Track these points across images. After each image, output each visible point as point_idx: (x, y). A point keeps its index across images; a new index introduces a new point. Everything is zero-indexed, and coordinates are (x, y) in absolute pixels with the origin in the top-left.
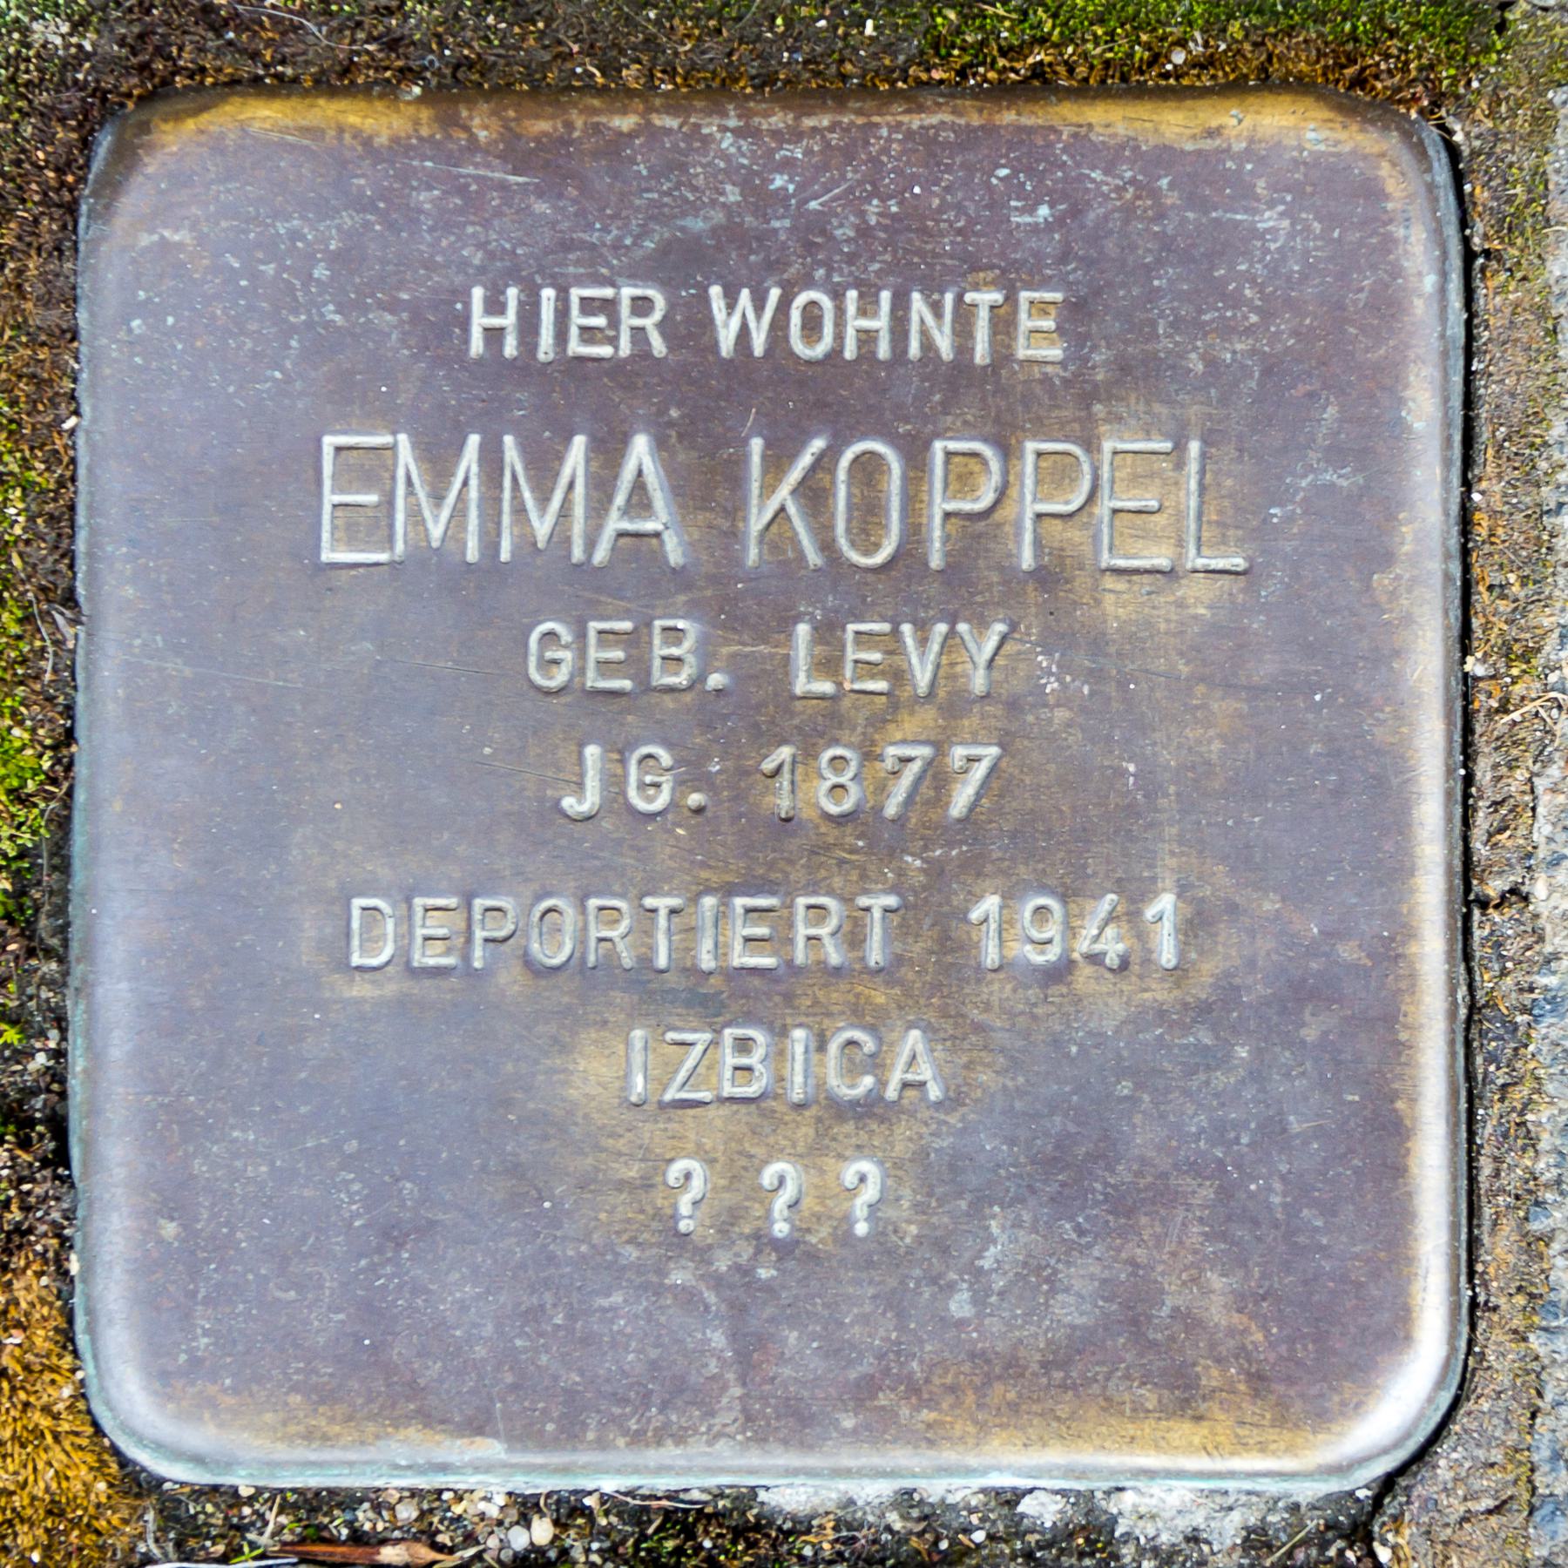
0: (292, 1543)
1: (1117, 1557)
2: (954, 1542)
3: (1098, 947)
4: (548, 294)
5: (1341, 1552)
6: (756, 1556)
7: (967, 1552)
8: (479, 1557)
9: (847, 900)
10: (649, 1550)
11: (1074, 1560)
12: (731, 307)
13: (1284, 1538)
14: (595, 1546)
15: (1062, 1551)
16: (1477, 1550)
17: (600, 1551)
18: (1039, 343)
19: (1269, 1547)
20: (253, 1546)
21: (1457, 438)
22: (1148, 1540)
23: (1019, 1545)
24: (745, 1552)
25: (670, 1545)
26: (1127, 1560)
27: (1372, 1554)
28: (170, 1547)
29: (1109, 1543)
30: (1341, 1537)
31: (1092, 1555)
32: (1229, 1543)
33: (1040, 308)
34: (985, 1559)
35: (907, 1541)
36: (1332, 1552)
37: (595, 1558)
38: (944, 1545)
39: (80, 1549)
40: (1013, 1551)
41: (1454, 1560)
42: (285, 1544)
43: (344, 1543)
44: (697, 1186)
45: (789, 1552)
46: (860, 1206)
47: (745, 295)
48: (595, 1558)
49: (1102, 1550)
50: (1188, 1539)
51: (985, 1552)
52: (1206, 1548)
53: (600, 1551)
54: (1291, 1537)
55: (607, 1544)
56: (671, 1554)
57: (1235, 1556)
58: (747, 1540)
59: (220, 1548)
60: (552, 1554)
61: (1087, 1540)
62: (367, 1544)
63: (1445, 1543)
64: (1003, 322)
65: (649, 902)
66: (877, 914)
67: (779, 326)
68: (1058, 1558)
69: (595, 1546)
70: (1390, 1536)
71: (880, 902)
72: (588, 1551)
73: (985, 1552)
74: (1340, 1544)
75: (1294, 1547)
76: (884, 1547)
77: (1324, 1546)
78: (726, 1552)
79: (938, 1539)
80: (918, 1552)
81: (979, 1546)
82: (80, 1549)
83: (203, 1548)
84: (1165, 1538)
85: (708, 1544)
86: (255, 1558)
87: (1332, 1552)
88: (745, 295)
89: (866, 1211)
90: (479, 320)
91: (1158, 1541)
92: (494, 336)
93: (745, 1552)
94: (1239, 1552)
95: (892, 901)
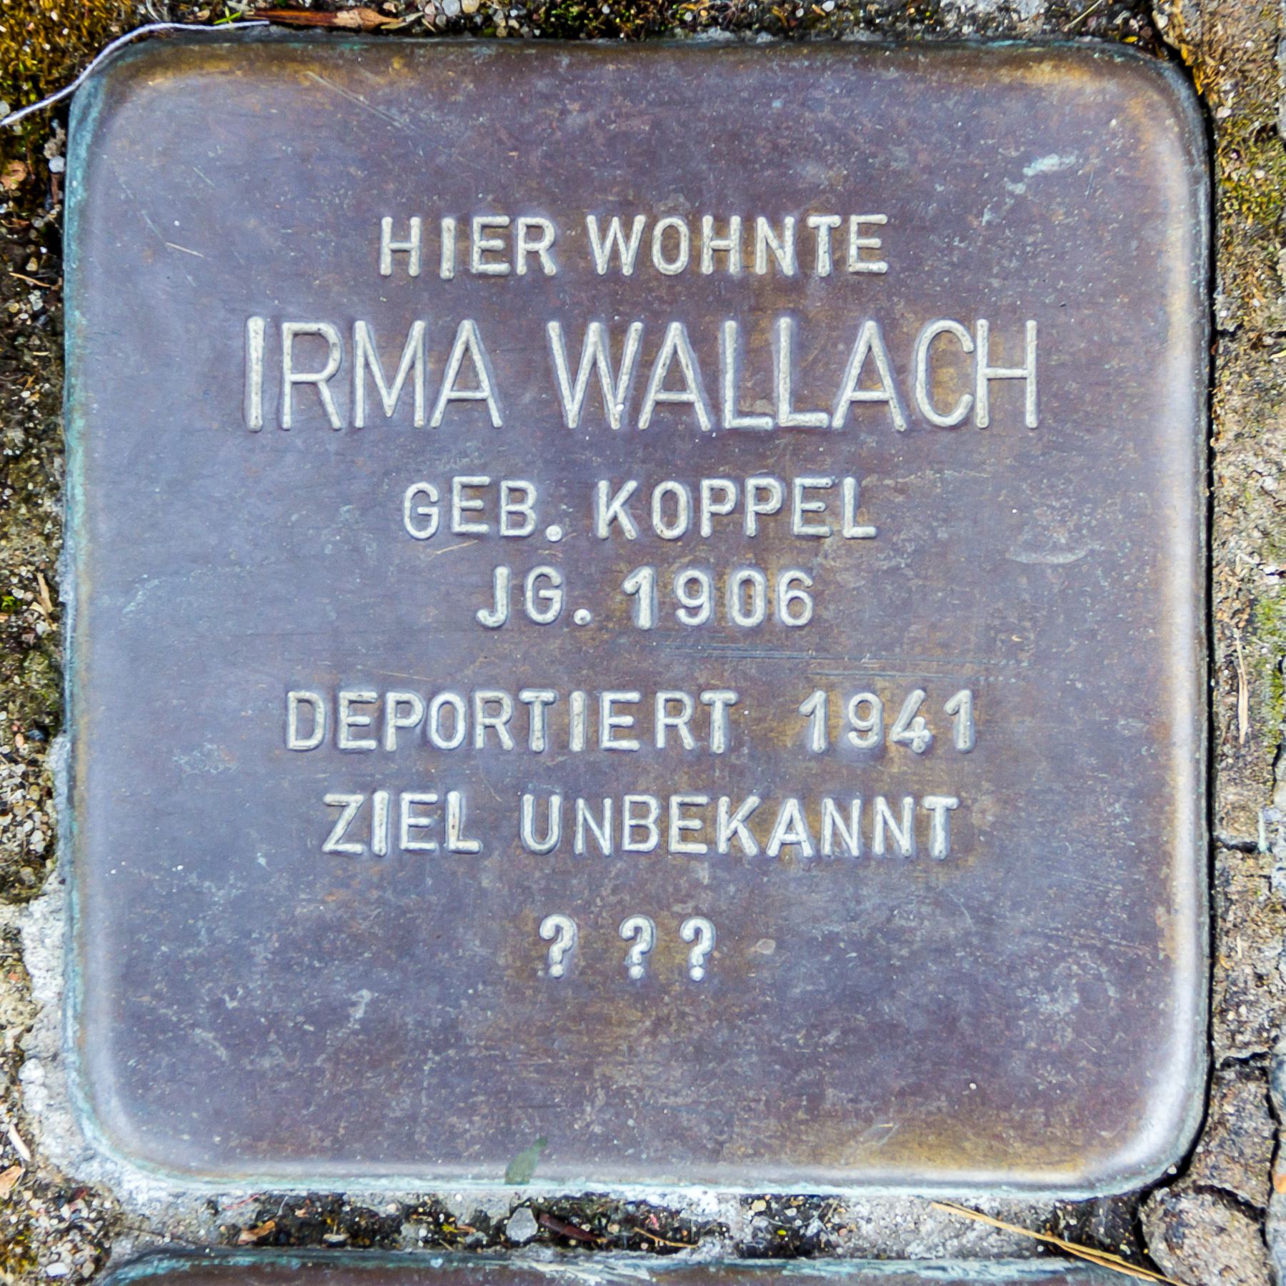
0: (265, 9)
1: (942, 23)
2: (808, 11)
3: (907, 735)
4: (448, 223)
5: (1126, 21)
6: (646, 19)
7: (819, 19)
8: (418, 22)
9: (696, 696)
10: (556, 16)
11: (906, 25)
12: (603, 237)
13: (1079, 9)
14: (514, 13)
15: (897, 19)
16: (1239, 20)
17: (517, 18)
18: (863, 256)
19: (1067, 17)
20: (232, 11)
21: (1204, 735)
22: (968, 10)
23: (861, 14)
24: (636, 16)
25: (575, 10)
26: (950, 25)
27: (1152, 23)
28: (165, 11)
29: (935, 12)
30: (1126, 8)
31: (922, 21)
32: (1034, 12)
33: (865, 230)
34: (833, 24)
35: (770, 10)
36: (1118, 21)
37: (513, 23)
38: (800, 13)
39: (91, 11)
40: (857, 18)
41: (1219, 27)
42: (258, 9)
43: (308, 9)
44: (566, 940)
45: (673, 15)
46: (697, 955)
47: (615, 223)
48: (513, 23)
49: (930, 18)
50: (1000, 9)
51: (834, 18)
52: (1015, 16)
53: (517, 18)
54: (1085, 8)
55: (524, 12)
56: (575, 19)
57: (1039, 23)
58: (638, 6)
59: (206, 13)
60: (478, 20)
61: (918, 10)
62: (326, 10)
63: (1212, 14)
64: (838, 238)
65: (526, 695)
66: (719, 707)
67: (645, 244)
68: (894, 23)
69: (514, 13)
70: (1166, 7)
71: (719, 699)
72: (507, 17)
73: (834, 18)
74: (1125, 14)
75: (1087, 17)
76: (750, 15)
77: (1112, 16)
78: (621, 16)
79: (795, 8)
80: (779, 19)
81: (828, 14)
82: (91, 11)
83: (193, 13)
84: (981, 8)
85: (606, 10)
86: (235, 21)
87: (1118, 21)
88: (615, 223)
89: (701, 961)
90: (387, 244)
91: (976, 10)
92: (400, 256)
93: (636, 16)
94: (1042, 19)
95: (731, 696)
